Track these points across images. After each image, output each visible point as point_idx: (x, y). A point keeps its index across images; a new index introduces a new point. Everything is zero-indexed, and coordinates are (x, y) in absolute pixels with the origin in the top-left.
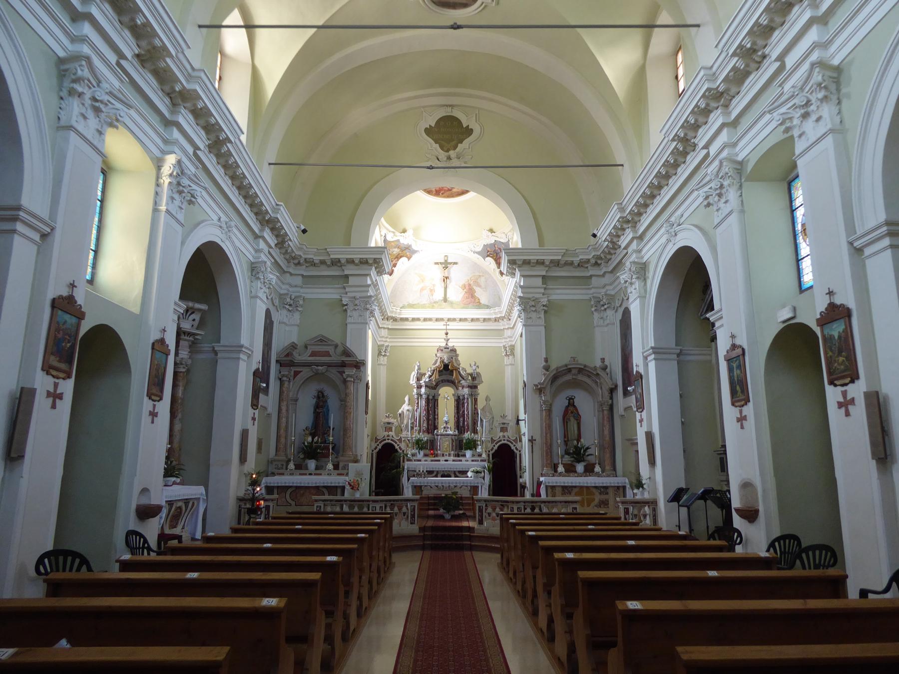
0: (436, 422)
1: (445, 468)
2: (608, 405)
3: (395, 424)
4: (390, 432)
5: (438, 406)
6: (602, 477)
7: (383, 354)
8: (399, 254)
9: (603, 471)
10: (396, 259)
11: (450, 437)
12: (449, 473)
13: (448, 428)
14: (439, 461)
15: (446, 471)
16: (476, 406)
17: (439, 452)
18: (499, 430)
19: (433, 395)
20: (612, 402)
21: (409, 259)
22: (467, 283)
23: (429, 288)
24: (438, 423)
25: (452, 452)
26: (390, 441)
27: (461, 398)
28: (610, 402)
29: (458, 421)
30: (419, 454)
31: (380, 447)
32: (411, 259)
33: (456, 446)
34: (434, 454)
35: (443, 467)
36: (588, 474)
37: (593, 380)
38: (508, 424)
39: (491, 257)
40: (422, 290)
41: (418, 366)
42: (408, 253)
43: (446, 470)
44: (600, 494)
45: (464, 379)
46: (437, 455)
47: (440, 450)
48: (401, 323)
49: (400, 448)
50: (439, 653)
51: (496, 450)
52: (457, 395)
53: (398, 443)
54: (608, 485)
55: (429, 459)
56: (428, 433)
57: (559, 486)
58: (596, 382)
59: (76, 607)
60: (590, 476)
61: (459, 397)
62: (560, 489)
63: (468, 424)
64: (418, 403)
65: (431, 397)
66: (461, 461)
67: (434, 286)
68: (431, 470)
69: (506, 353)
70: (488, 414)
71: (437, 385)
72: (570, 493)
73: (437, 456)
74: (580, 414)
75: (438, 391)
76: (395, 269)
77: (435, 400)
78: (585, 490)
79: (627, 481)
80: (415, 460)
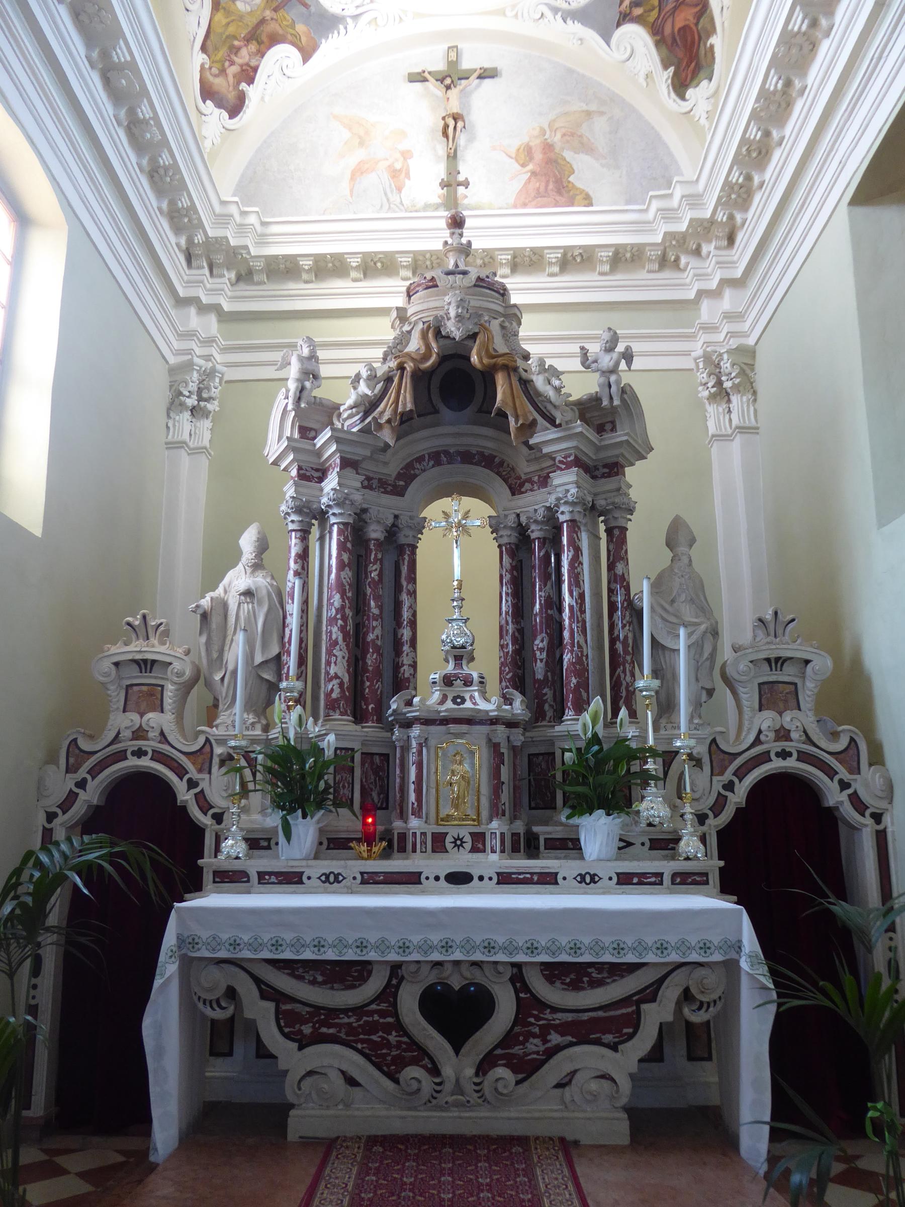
0: (406, 660)
1: (447, 946)
3: (177, 665)
4: (150, 715)
5: (412, 579)
7: (191, 402)
8: (263, 21)
10: (253, 47)
11: (482, 730)
12: (479, 978)
13: (468, 682)
15: (457, 963)
16: (619, 568)
17: (414, 823)
18: (750, 696)
19: (390, 521)
21: (307, 55)
22: (538, 141)
23: (387, 163)
24: (414, 666)
25: (495, 824)
26: (146, 763)
27: (535, 532)
29: (518, 652)
30: (288, 836)
31: (739, 796)
33: (516, 789)
34: (387, 836)
35: (435, 938)
38: (807, 662)
39: (639, 20)
40: (358, 172)
41: (301, 359)
42: (300, 28)
43: (457, 956)
45: (552, 421)
47: (417, 813)
49: (855, 800)
50: (492, 1180)
51: (738, 810)
52: (511, 520)
53: (193, 773)
55: (352, 867)
56: (359, 717)
61: (522, 530)
63: (580, 660)
64: (304, 556)
65: (375, 533)
66: (548, 879)
67: (405, 159)
68: (350, 955)
69: (719, 383)
70: (687, 612)
71: (408, 475)
73: (402, 849)
76: (253, 92)
77: (401, 549)
80: (261, 875)
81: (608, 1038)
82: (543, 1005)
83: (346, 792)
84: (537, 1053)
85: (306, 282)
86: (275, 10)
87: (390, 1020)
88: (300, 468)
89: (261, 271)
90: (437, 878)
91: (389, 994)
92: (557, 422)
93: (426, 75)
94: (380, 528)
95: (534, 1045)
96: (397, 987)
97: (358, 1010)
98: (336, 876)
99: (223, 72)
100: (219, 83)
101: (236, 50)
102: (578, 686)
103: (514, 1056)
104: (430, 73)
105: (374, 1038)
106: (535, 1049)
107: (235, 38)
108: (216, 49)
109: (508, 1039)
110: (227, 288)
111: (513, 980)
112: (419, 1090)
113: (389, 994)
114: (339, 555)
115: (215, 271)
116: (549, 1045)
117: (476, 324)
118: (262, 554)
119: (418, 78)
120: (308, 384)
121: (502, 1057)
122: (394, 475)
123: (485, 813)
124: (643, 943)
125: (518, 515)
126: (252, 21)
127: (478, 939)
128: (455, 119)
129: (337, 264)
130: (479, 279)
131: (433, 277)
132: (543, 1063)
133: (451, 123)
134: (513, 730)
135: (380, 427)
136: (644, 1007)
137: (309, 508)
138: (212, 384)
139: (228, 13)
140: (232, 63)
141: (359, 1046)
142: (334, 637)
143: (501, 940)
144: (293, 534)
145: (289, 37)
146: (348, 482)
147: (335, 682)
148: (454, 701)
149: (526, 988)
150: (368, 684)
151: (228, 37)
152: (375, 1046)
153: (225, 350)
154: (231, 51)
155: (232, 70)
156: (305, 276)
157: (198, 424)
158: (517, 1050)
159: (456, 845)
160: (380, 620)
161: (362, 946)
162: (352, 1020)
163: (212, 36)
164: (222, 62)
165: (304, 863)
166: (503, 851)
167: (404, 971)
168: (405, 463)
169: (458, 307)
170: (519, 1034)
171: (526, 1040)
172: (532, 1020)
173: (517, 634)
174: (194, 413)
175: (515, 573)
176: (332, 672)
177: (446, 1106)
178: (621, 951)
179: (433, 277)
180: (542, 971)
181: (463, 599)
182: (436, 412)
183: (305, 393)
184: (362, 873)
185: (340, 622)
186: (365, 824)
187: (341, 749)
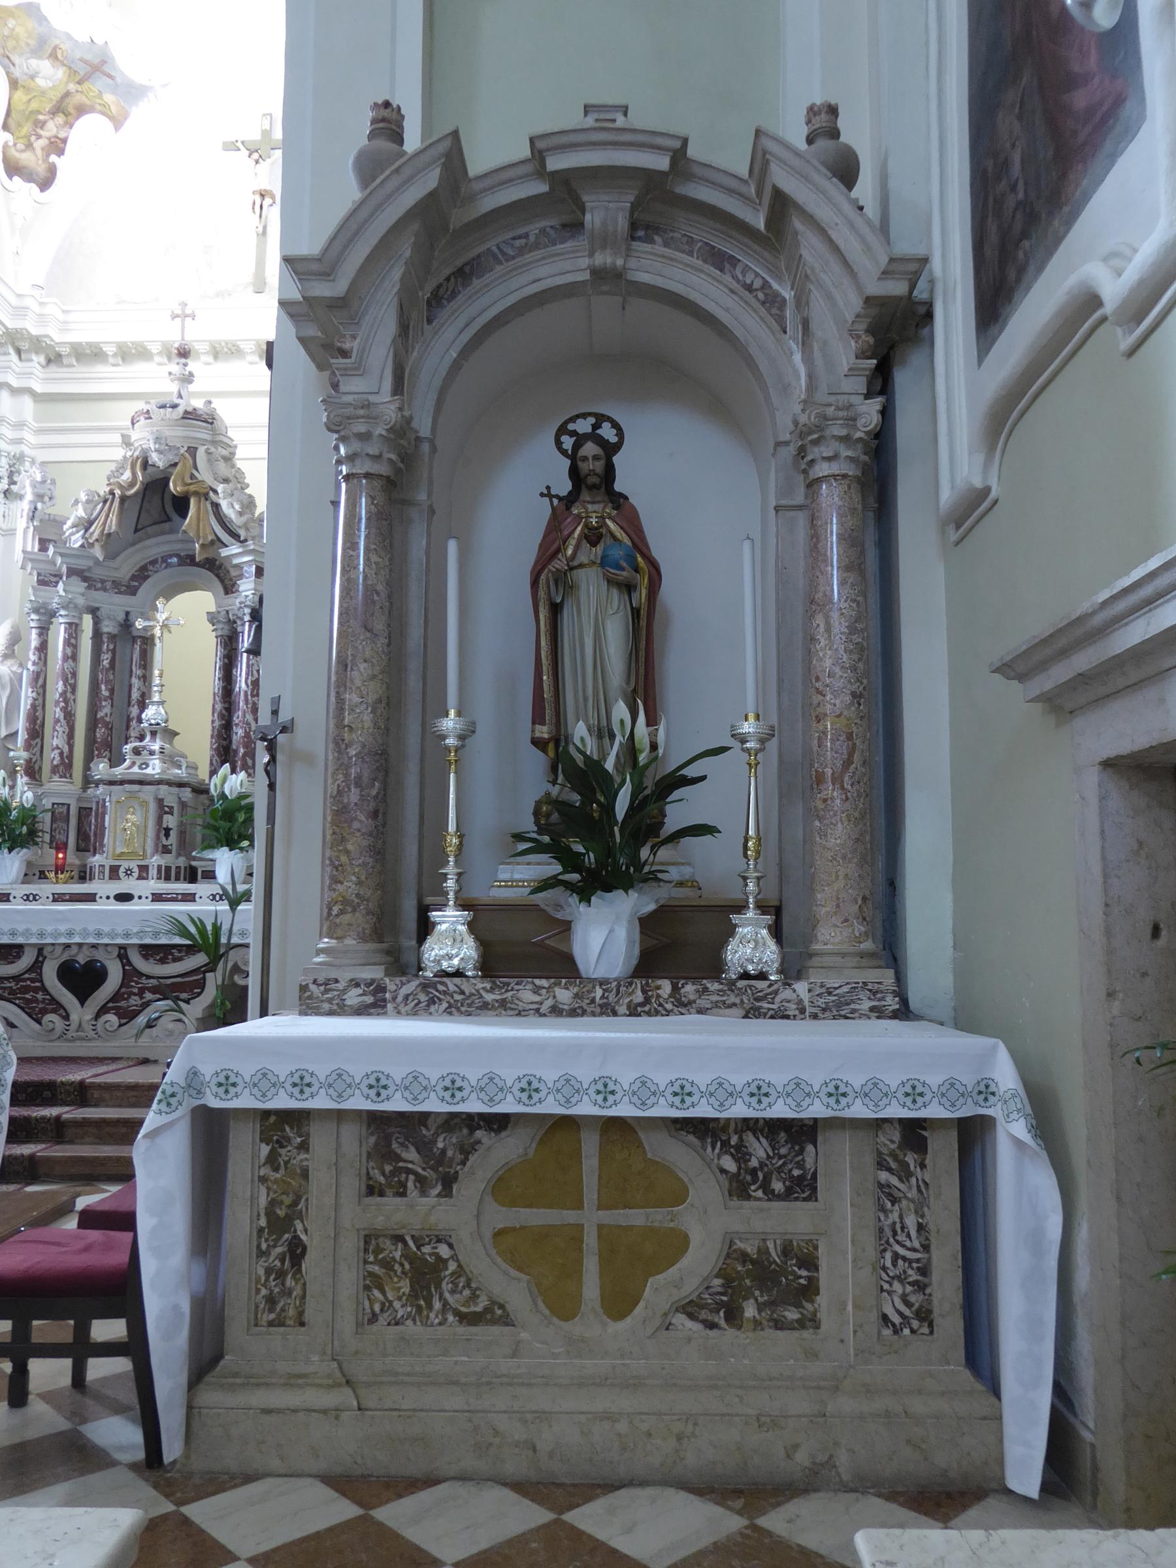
1: (70, 934)
2: (846, 439)
6: (781, 1015)
8: (67, 94)
9: (791, 970)
10: (60, 119)
11: (148, 792)
14: (90, 898)
15: (80, 945)
19: (121, 617)
20: (887, 413)
21: (118, 122)
28: (870, 412)
32: (128, 123)
35: (63, 928)
36: (666, 987)
37: (749, 288)
42: (109, 98)
44: (739, 1188)
45: (235, 536)
46: (84, 875)
48: (80, 370)
54: (817, 1110)
55: (46, 889)
57: (340, 1116)
58: (773, 302)
59: (465, 1037)
60: (683, 1005)
62: (353, 1140)
72: (448, 1183)
74: (656, 552)
75: (149, 611)
78: (590, 1144)
79: (1006, 1076)
81: (184, 996)
82: (141, 974)
83: (61, 837)
84: (136, 1006)
85: (114, 365)
86: (79, 83)
87: (38, 984)
88: (39, 574)
89: (69, 354)
90: (108, 898)
91: (37, 966)
92: (242, 538)
93: (239, 145)
94: (111, 623)
95: (135, 1001)
96: (42, 963)
97: (16, 978)
98: (34, 896)
99: (29, 146)
100: (26, 158)
101: (43, 124)
102: (245, 754)
103: (120, 1007)
104: (243, 143)
105: (27, 996)
106: (135, 1003)
107: (39, 112)
108: (20, 125)
109: (116, 997)
110: (38, 371)
111: (120, 956)
112: (53, 1029)
113: (37, 966)
114: (64, 649)
115: (23, 356)
116: (144, 1000)
117: (177, 455)
118: (14, 645)
119: (231, 146)
120: (39, 505)
121: (113, 1008)
122: (128, 578)
123: (149, 850)
124: (649, 1084)
125: (227, 612)
126: (55, 96)
127: (91, 928)
128: (263, 196)
129: (141, 350)
130: (186, 412)
131: (148, 411)
132: (140, 1012)
133: (258, 200)
134: (182, 789)
135: (92, 545)
136: (208, 975)
137: (46, 609)
138: (22, 468)
139: (27, 89)
140: (39, 137)
141: (17, 1002)
142: (57, 716)
143: (106, 929)
144: (34, 630)
145: (98, 107)
146: (72, 589)
147: (57, 752)
148: (140, 768)
149: (129, 963)
150: (96, 752)
151: (31, 112)
152: (28, 1001)
153: (40, 431)
154: (36, 126)
155: (39, 144)
156: (111, 360)
157: (12, 506)
158: (123, 1004)
159: (127, 874)
160: (110, 701)
161: (13, 934)
162: (12, 984)
163: (13, 114)
164: (28, 137)
165: (9, 886)
166: (159, 878)
167: (45, 953)
168: (138, 567)
169: (155, 443)
170: (124, 993)
171: (129, 997)
172: (133, 984)
173: (224, 712)
174: (8, 495)
175: (226, 660)
176: (54, 744)
177: (73, 1040)
178: (756, 1091)
179: (148, 411)
180: (140, 952)
181: (162, 686)
182: (169, 519)
183: (37, 513)
184: (53, 894)
185: (62, 704)
186: (57, 858)
187: (58, 804)
